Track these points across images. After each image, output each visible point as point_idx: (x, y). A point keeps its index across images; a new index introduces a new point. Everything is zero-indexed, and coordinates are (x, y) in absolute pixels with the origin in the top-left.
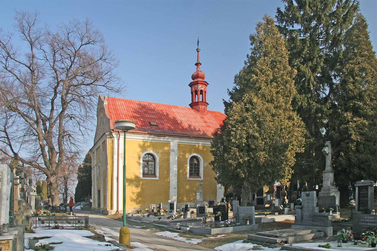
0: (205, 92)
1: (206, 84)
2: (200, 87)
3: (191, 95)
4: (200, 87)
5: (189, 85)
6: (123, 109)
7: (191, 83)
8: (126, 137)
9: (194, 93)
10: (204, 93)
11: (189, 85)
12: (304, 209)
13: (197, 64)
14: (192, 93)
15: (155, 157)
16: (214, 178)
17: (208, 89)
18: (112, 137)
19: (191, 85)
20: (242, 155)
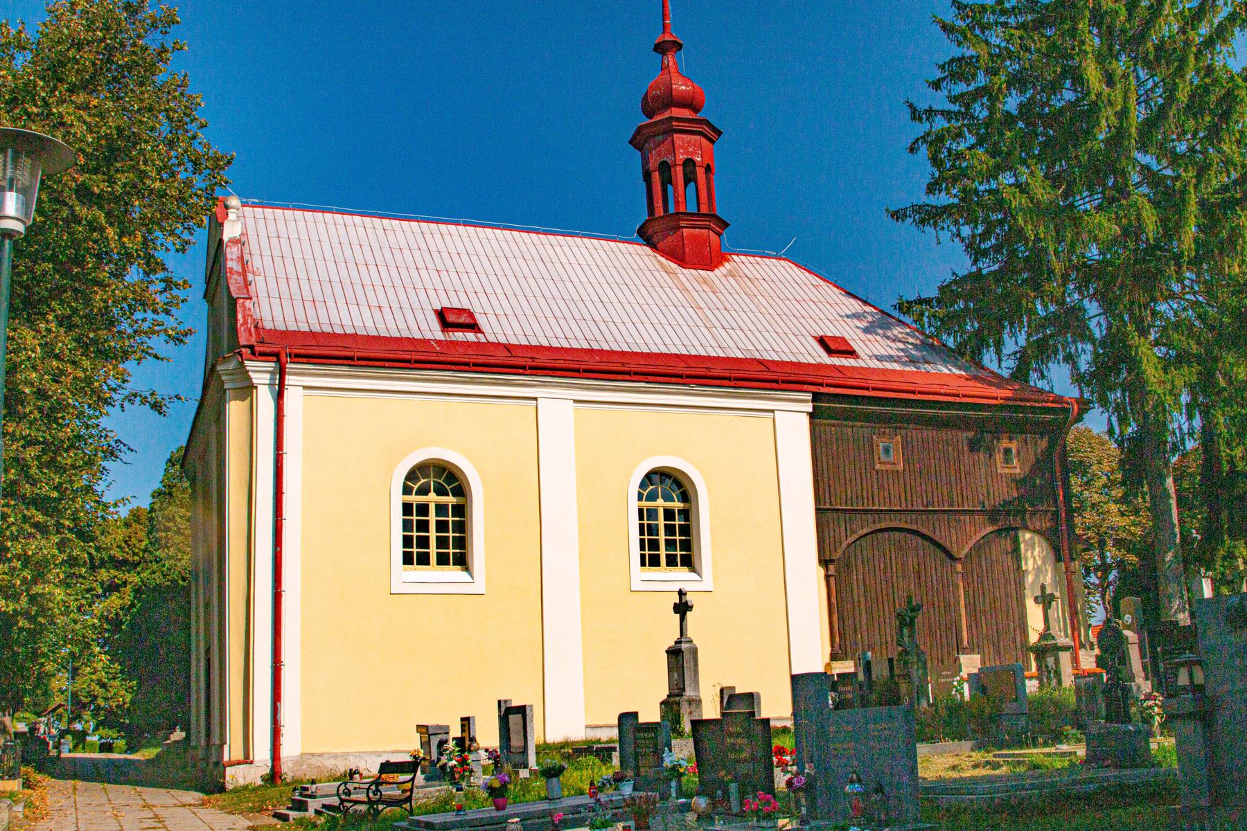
0: (708, 169)
1: (713, 133)
2: (686, 147)
3: (644, 184)
4: (686, 147)
5: (631, 142)
6: (273, 234)
7: (640, 129)
8: (286, 383)
9: (656, 177)
10: (700, 172)
11: (631, 142)
12: (1223, 716)
13: (661, 48)
14: (647, 176)
15: (688, 486)
16: (1238, 59)
17: (721, 153)
18: (247, 390)
19: (638, 141)
20: (1156, 724)
